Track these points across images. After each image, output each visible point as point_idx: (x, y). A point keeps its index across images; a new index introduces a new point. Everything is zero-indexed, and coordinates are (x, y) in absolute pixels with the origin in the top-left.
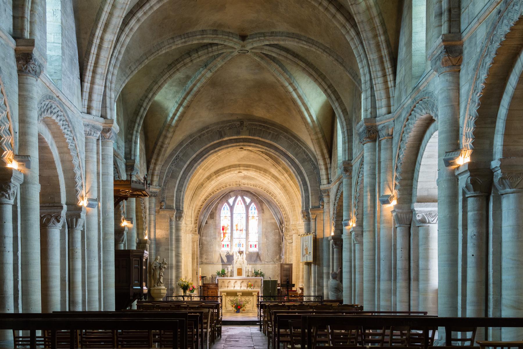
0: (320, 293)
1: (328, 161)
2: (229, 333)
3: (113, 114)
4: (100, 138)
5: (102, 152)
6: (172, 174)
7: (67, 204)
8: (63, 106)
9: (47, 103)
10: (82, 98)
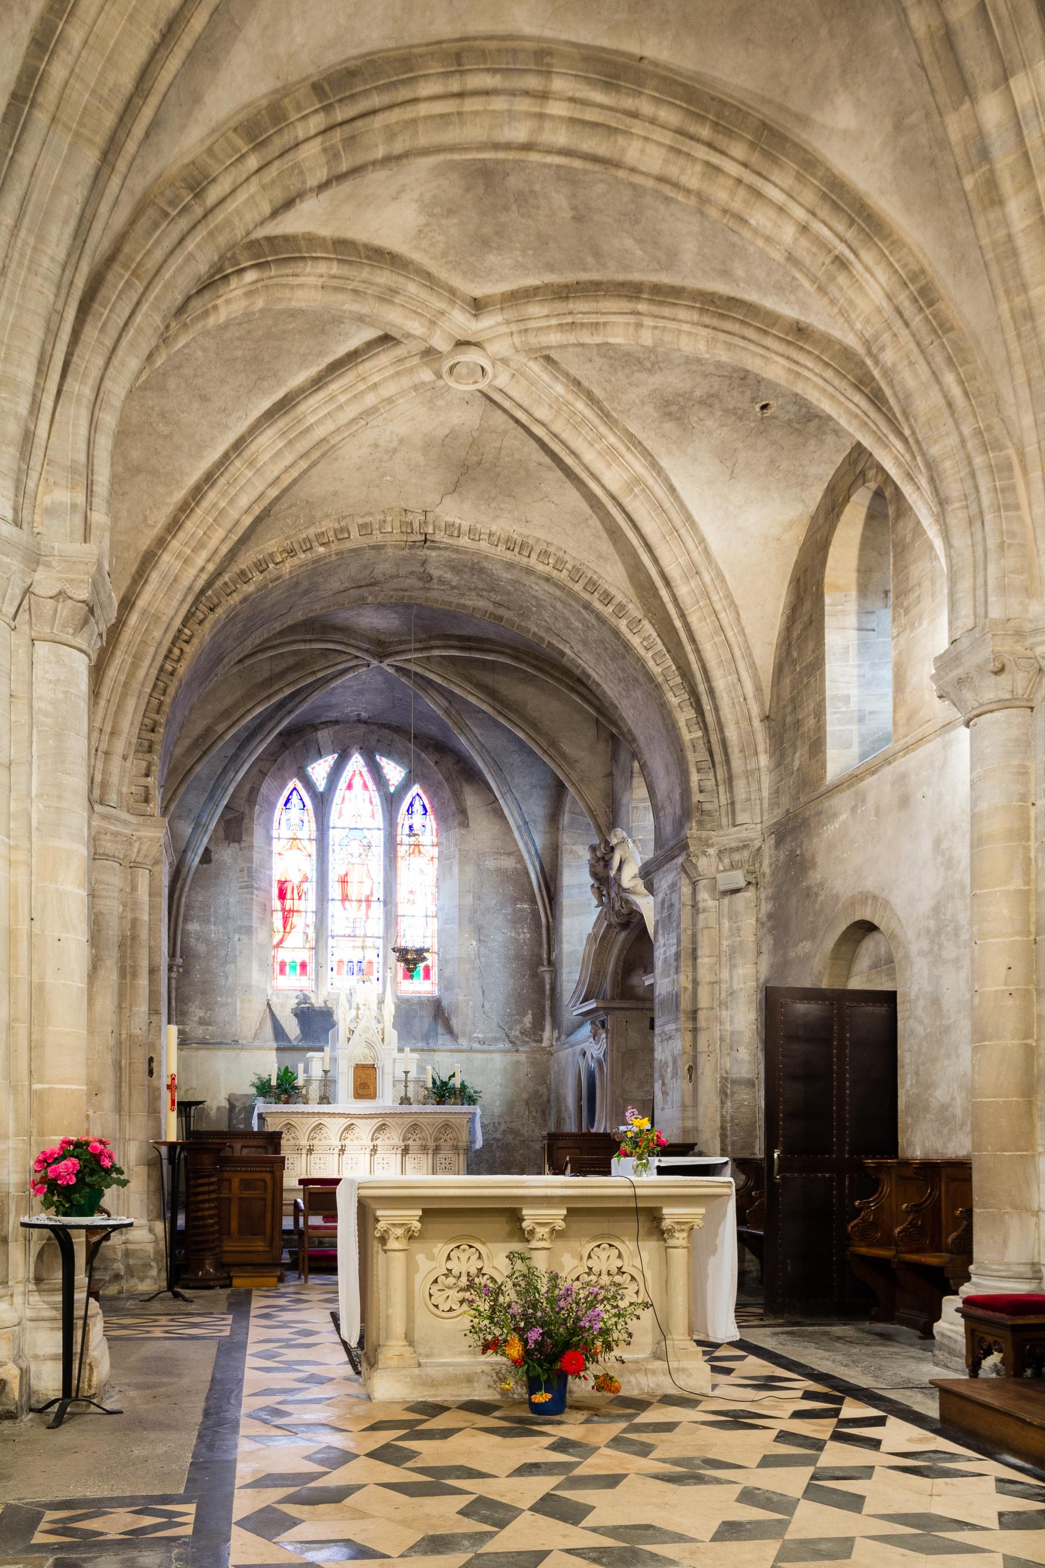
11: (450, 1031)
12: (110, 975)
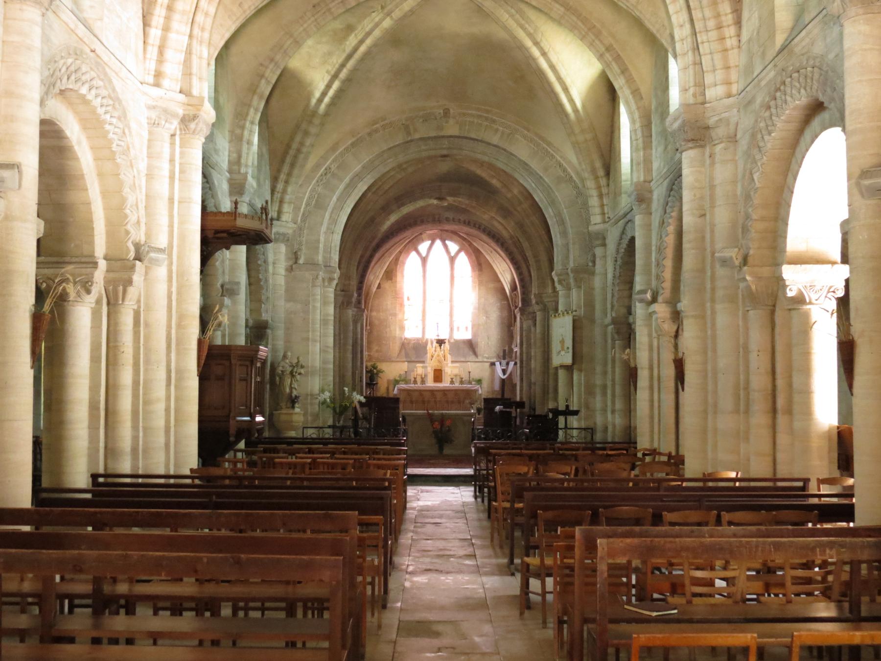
0: (590, 424)
1: (603, 182)
2: (421, 503)
3: (203, 87)
4: (178, 132)
5: (181, 158)
6: (317, 201)
7: (106, 258)
8: (104, 69)
9: (70, 61)
10: (145, 58)
11: (475, 354)
12: (337, 348)
